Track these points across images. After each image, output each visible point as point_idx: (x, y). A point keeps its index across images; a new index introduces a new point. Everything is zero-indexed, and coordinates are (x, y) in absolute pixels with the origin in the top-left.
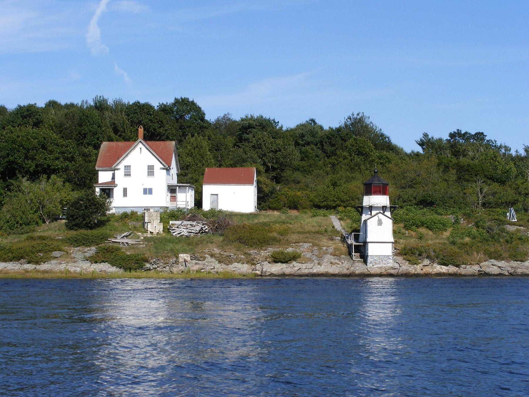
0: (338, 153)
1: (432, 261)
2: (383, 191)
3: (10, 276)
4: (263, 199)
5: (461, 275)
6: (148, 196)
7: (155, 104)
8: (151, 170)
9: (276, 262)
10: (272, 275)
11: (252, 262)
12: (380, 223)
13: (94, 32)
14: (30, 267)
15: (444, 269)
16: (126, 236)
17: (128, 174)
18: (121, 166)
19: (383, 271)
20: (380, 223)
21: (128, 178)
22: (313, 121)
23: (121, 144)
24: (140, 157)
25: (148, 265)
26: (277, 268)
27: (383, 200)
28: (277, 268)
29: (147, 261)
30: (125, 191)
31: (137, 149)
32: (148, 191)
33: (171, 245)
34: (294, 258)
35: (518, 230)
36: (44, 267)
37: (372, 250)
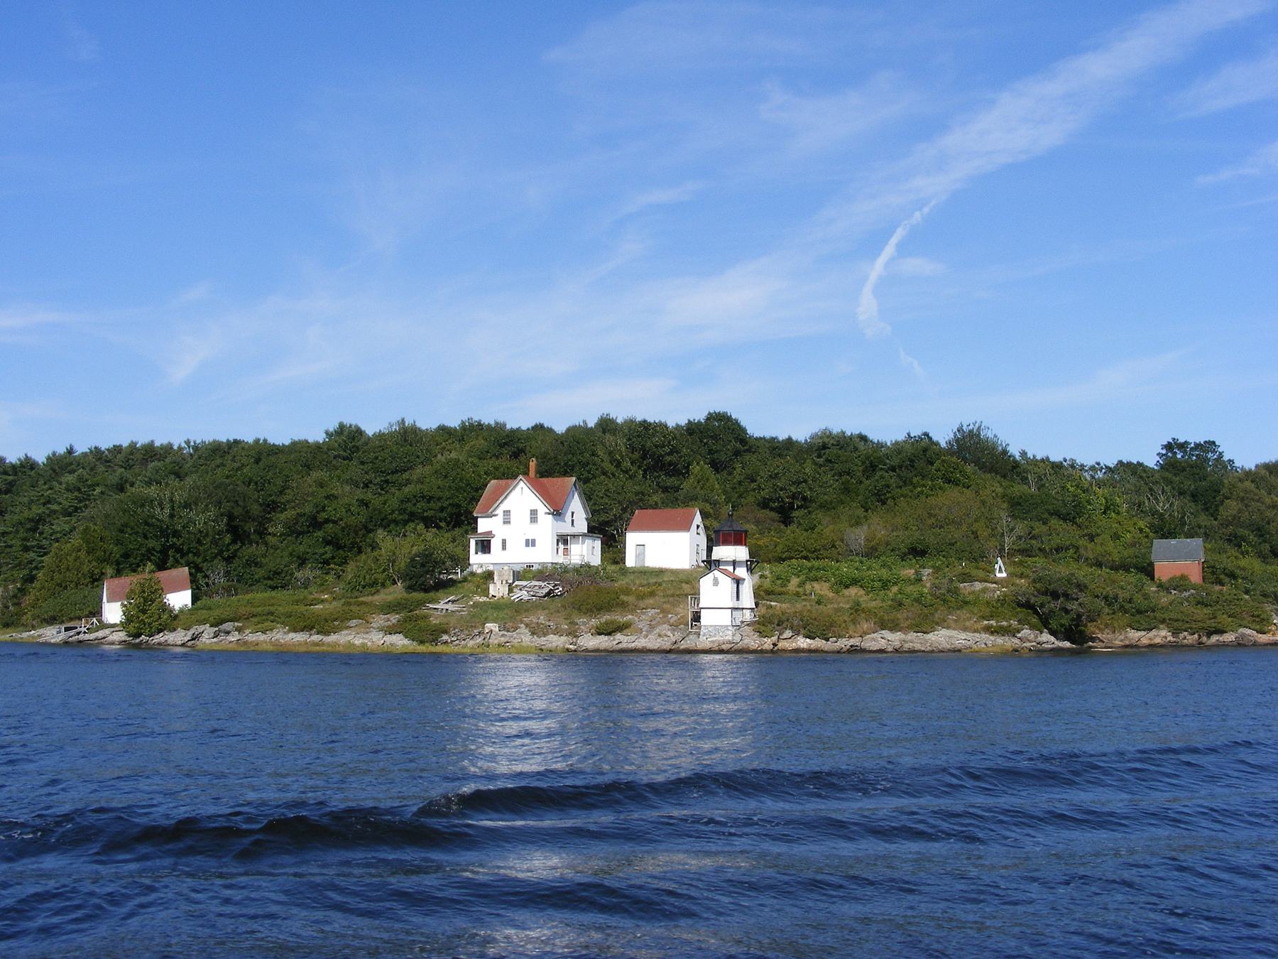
0: (915, 480)
2: (737, 539)
4: (195, 599)
5: (863, 651)
6: (530, 548)
7: (671, 424)
8: (534, 514)
9: (600, 634)
10: (587, 650)
11: (573, 634)
12: (716, 582)
13: (867, 305)
14: (316, 638)
15: (803, 642)
16: (453, 602)
17: (507, 522)
18: (500, 511)
19: (715, 647)
20: (716, 582)
21: (507, 526)
22: (926, 434)
23: (503, 482)
24: (521, 498)
25: (445, 637)
26: (602, 642)
27: (741, 553)
28: (602, 642)
29: (446, 632)
30: (504, 542)
31: (518, 489)
32: (530, 543)
34: (621, 628)
35: (984, 590)
36: (332, 638)
37: (707, 618)
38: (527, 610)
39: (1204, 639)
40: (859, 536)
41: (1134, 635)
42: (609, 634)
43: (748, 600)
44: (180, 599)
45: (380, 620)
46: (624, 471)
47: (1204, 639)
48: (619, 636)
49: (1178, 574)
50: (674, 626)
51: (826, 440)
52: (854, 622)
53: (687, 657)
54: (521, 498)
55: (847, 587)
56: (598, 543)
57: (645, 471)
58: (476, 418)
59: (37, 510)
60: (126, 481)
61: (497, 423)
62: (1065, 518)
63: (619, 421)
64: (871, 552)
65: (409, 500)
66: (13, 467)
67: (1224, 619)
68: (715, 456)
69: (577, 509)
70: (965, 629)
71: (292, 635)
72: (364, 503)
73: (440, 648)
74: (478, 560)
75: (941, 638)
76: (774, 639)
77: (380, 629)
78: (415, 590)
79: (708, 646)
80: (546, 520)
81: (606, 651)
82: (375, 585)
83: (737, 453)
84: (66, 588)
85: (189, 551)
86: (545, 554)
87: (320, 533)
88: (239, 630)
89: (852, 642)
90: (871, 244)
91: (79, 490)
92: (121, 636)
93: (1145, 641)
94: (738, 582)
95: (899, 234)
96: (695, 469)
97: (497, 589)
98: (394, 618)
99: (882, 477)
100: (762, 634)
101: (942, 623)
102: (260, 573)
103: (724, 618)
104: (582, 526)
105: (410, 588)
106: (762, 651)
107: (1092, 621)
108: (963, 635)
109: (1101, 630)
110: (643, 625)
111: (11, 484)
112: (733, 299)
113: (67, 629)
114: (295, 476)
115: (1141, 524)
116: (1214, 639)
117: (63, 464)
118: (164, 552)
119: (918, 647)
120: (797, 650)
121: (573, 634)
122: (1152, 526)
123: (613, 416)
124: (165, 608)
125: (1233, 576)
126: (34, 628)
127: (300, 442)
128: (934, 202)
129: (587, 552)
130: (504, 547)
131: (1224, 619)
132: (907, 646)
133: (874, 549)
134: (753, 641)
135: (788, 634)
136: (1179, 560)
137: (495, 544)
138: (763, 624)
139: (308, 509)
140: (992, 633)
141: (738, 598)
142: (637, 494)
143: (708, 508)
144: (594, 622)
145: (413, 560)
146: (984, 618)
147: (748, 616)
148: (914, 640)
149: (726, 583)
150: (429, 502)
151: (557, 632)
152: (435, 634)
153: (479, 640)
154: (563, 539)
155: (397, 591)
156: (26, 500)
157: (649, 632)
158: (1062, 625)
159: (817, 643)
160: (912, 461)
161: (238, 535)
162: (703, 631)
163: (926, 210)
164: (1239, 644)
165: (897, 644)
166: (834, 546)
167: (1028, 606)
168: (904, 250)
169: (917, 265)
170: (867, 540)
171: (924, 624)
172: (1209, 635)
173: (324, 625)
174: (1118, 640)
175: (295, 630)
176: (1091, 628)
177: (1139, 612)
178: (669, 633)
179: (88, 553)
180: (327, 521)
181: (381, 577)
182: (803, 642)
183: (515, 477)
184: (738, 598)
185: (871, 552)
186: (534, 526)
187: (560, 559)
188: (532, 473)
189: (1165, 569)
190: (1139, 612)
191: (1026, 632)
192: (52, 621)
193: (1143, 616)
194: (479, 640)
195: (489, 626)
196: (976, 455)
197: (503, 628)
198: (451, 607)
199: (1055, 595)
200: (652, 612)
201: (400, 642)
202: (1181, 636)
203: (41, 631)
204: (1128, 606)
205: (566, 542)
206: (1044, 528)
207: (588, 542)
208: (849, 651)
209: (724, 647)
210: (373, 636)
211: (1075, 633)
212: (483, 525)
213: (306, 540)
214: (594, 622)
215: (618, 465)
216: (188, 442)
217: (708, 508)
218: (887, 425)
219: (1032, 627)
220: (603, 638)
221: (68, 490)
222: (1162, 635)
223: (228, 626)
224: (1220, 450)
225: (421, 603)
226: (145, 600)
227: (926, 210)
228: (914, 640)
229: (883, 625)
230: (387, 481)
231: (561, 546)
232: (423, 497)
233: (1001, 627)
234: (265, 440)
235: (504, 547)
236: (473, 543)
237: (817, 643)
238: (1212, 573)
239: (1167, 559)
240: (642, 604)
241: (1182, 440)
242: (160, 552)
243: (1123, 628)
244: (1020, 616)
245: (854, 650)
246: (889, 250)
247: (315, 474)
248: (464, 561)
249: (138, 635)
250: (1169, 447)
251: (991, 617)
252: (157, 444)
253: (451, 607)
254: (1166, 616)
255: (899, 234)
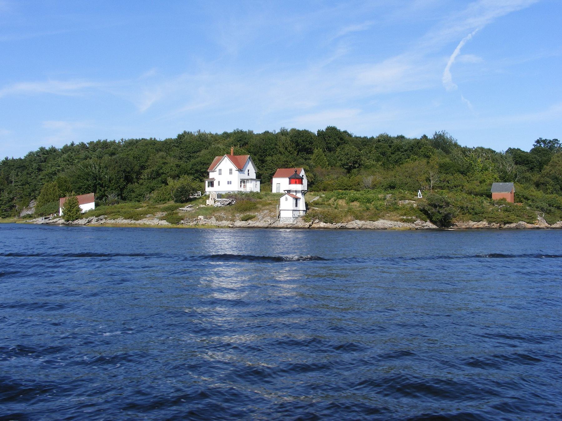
1: (320, 220)
3: (118, 226)
4: (97, 205)
8: (231, 170)
12: (286, 199)
13: (447, 76)
14: (133, 222)
15: (322, 225)
16: (190, 207)
17: (220, 174)
18: (217, 170)
20: (286, 199)
25: (182, 221)
26: (244, 224)
28: (244, 224)
29: (183, 219)
30: (219, 182)
31: (225, 160)
32: (229, 183)
33: (380, 202)
36: (139, 222)
37: (283, 214)
38: (218, 211)
39: (502, 226)
40: (369, 180)
41: (472, 224)
42: (246, 220)
43: (302, 206)
44: (87, 207)
45: (159, 214)
46: (269, 153)
47: (502, 226)
48: (250, 221)
49: (502, 198)
50: (272, 217)
51: (380, 138)
52: (345, 216)
53: (275, 230)
54: (226, 164)
55: (353, 201)
56: (259, 183)
57: (298, 152)
58: (240, 129)
59: (54, 169)
60: (88, 157)
61: (249, 131)
62: (462, 173)
63: (289, 130)
64: (374, 187)
65: (195, 165)
66: (47, 151)
67: (513, 217)
68: (329, 145)
69: (251, 170)
70: (391, 220)
71: (124, 220)
72: (178, 166)
73: (180, 226)
74: (208, 189)
75: (380, 223)
76: (310, 223)
77: (158, 218)
78: (178, 202)
79: (282, 225)
80: (236, 173)
81: (243, 227)
82: (164, 200)
83: (338, 144)
84: (49, 202)
85: (105, 186)
86: (235, 187)
87: (160, 179)
88: (106, 218)
89: (343, 224)
90: (448, 49)
91: (68, 161)
92: (62, 221)
93: (475, 226)
94: (297, 199)
95: (462, 44)
96: (316, 151)
97: (209, 202)
98: (165, 214)
99: (398, 155)
100: (305, 221)
101: (383, 217)
102: (133, 195)
103: (290, 214)
104: (253, 176)
105: (176, 201)
106: (304, 228)
107: (455, 217)
108: (390, 222)
109: (458, 221)
110: (260, 217)
111: (46, 158)
112: (386, 73)
113: (45, 218)
114: (152, 155)
115: (495, 176)
116: (507, 226)
117: (68, 149)
118: (95, 186)
119: (368, 227)
120: (319, 228)
121: (233, 220)
122: (500, 177)
123: (286, 128)
124: (79, 210)
125: (527, 199)
126: (35, 218)
127: (169, 139)
128: (477, 30)
129: (254, 187)
130: (219, 185)
131: (513, 217)
132: (364, 227)
133: (375, 185)
134: (301, 224)
135: (317, 221)
136: (504, 192)
137: (216, 183)
138: (306, 218)
139: (155, 168)
140: (404, 222)
141: (296, 206)
142: (285, 161)
143: (307, 168)
144: (242, 215)
145: (177, 190)
146: (402, 215)
147: (302, 213)
148: (368, 224)
149: (291, 200)
150: (203, 165)
151: (227, 219)
152: (177, 220)
153: (195, 223)
154: (243, 181)
155: (172, 203)
156: (50, 165)
157: (261, 220)
158: (438, 219)
159: (328, 225)
160: (412, 148)
161: (128, 179)
162: (281, 219)
163: (474, 33)
164: (517, 228)
165: (360, 226)
166: (359, 184)
167: (424, 211)
168: (464, 51)
169: (470, 58)
170: (373, 182)
171: (373, 218)
172: (505, 224)
173: (136, 217)
174: (464, 225)
175: (125, 219)
176: (454, 220)
177: (476, 214)
178: (269, 220)
179: (59, 187)
180: (163, 173)
181: (167, 197)
182: (322, 225)
183: (223, 155)
184: (296, 206)
185: (374, 187)
186: (231, 175)
187: (242, 189)
188: (232, 154)
189: (496, 195)
190: (476, 214)
191: (418, 221)
192: (41, 215)
193: (477, 215)
194: (195, 223)
195: (200, 217)
196: (442, 144)
197: (206, 218)
198: (189, 209)
199: (435, 206)
200: (266, 211)
201: (164, 223)
202: (492, 224)
203: (37, 219)
204: (471, 211)
205: (244, 182)
206: (452, 177)
207: (254, 182)
208: (340, 228)
209: (289, 226)
210: (154, 221)
211: (444, 223)
212: (211, 175)
213: (155, 181)
214: (242, 215)
215: (286, 149)
216: (122, 140)
217: (307, 168)
218: (413, 133)
219: (422, 219)
220: (244, 222)
221: (64, 161)
222: (484, 224)
223: (102, 217)
224: (560, 143)
225: (177, 208)
226: (71, 206)
227: (474, 33)
228: (368, 224)
229: (357, 218)
230: (190, 156)
231: (243, 184)
232: (201, 163)
233: (408, 219)
234: (155, 139)
235: (219, 185)
236: (207, 182)
237: (328, 225)
238: (518, 197)
239: (497, 191)
240: (263, 208)
241: (544, 139)
242: (93, 186)
243: (468, 220)
244: (418, 215)
245: (342, 228)
246: (457, 51)
247: (161, 154)
248: (203, 191)
249: (68, 221)
250: (538, 142)
251: (405, 215)
252: (108, 141)
253: (189, 209)
254: (487, 216)
255: (462, 44)
